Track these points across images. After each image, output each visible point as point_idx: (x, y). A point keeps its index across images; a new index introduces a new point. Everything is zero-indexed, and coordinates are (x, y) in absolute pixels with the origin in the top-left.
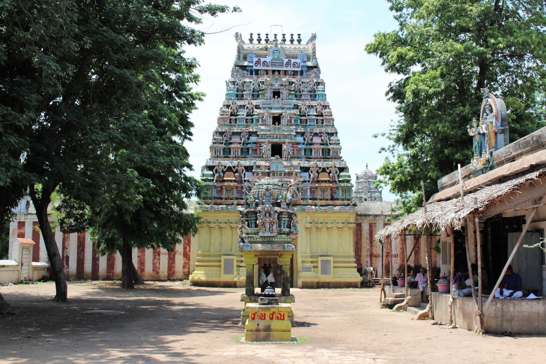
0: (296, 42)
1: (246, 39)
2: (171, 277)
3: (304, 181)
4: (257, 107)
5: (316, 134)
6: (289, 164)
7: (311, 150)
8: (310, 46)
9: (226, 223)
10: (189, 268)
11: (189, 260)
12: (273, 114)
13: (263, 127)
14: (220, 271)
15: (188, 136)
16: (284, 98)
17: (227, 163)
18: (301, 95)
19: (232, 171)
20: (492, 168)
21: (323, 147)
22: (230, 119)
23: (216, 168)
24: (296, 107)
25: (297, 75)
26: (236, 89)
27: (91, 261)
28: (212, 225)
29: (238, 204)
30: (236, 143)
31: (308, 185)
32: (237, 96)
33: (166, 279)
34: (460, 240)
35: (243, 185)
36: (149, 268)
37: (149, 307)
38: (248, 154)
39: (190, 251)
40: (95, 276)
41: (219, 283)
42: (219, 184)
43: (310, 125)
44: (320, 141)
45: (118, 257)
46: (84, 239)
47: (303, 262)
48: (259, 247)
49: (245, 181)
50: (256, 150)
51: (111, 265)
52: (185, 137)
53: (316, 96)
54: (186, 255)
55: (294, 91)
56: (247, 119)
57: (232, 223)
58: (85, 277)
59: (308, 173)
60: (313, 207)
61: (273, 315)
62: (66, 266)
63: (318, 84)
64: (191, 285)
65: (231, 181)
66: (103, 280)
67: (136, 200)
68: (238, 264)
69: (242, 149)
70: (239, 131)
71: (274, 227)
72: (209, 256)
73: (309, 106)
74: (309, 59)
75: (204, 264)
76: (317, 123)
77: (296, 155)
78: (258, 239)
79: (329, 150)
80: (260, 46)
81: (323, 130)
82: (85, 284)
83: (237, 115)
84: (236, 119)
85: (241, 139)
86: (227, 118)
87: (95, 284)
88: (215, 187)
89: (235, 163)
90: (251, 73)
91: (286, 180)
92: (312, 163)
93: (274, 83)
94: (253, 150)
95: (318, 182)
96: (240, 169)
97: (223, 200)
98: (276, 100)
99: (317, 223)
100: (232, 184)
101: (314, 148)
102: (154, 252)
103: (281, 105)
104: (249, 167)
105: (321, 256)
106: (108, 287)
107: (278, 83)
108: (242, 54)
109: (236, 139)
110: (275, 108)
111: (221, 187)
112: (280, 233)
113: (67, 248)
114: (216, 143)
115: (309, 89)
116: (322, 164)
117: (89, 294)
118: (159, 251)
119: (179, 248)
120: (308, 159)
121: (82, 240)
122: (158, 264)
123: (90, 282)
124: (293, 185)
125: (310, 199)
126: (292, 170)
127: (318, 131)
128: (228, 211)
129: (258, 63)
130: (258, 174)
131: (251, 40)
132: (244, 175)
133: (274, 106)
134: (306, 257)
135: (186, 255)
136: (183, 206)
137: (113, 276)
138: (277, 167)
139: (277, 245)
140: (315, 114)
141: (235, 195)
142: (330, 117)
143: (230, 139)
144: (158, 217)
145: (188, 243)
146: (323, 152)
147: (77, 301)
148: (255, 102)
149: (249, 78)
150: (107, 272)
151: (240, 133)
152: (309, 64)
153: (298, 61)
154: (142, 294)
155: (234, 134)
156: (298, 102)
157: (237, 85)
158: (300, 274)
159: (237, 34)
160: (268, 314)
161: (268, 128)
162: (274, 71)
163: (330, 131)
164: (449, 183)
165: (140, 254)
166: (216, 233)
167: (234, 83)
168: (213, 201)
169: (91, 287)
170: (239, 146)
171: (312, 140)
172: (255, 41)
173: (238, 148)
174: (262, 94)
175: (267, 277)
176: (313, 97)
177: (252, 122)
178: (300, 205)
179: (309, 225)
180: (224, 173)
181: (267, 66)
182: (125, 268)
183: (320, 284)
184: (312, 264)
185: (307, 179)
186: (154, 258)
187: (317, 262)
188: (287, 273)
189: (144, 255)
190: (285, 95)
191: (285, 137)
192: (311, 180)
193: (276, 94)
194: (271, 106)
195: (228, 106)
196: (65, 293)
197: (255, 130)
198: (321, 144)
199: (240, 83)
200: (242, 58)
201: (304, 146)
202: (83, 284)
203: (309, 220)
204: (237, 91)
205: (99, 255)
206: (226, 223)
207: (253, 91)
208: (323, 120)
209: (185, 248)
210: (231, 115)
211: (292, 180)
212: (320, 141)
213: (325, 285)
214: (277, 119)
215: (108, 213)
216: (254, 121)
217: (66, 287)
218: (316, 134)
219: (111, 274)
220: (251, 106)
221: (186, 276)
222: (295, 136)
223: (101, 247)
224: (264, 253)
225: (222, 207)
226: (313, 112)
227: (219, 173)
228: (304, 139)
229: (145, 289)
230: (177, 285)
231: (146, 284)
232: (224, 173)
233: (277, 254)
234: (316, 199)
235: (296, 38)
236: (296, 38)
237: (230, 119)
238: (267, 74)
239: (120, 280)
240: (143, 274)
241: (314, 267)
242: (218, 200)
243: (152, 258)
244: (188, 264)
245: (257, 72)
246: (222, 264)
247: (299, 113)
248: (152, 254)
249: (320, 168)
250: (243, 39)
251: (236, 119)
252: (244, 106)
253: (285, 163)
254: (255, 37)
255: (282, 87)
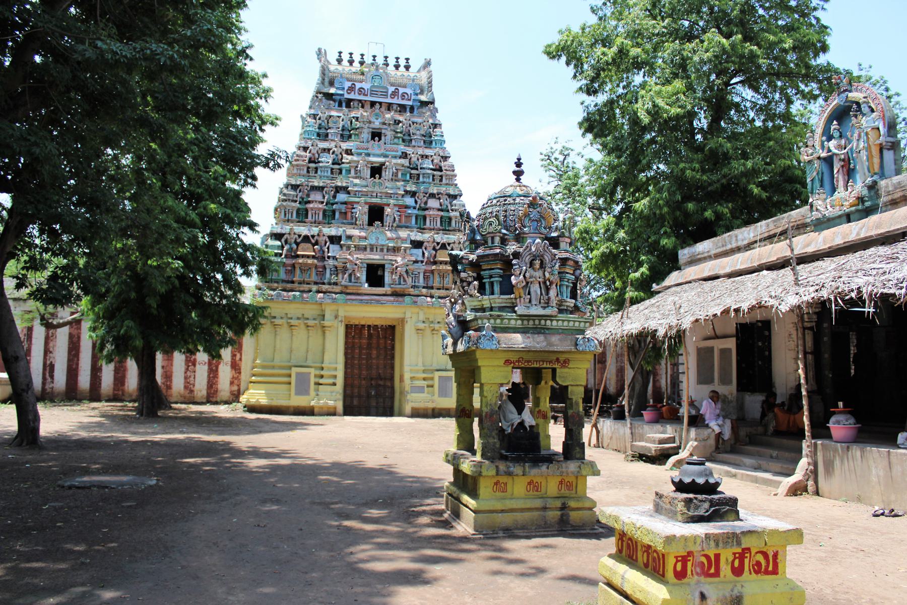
0: (402, 69)
1: (332, 58)
2: (211, 398)
3: (416, 262)
4: (349, 152)
5: (432, 196)
6: (394, 236)
7: (425, 218)
8: (424, 75)
9: (298, 318)
10: (239, 386)
11: (240, 373)
12: (372, 163)
13: (357, 181)
14: (290, 390)
15: (249, 181)
16: (388, 141)
17: (303, 230)
18: (411, 140)
19: (310, 242)
20: (868, 212)
21: (442, 213)
22: (308, 168)
23: (285, 237)
24: (405, 155)
25: (405, 111)
26: (317, 126)
27: (89, 372)
28: (277, 321)
29: (318, 292)
30: (317, 201)
31: (422, 267)
32: (318, 135)
33: (204, 401)
34: (760, 344)
35: (326, 263)
36: (178, 384)
37: (199, 460)
38: (334, 218)
39: (241, 359)
40: (94, 395)
41: (288, 408)
42: (289, 261)
43: (424, 182)
44: (438, 206)
45: (132, 366)
46: (79, 338)
47: (412, 378)
48: (518, 340)
49: (329, 257)
50: (346, 213)
51: (120, 377)
52: (246, 184)
53: (431, 142)
54: (235, 366)
55: (401, 133)
56: (332, 169)
57: (308, 319)
58: (78, 397)
59: (420, 250)
60: (429, 299)
61: (741, 557)
62: (49, 380)
63: (436, 126)
64: (245, 411)
65: (308, 257)
66: (108, 401)
67: (172, 268)
68: (317, 380)
69: (325, 211)
70: (321, 185)
71: (553, 293)
72: (273, 367)
73: (422, 156)
74: (422, 93)
75: (265, 378)
76: (433, 180)
77: (403, 223)
78: (513, 322)
79: (450, 219)
80: (354, 69)
81: (443, 189)
82: (79, 408)
83: (319, 162)
84: (316, 168)
85: (324, 197)
86: (303, 166)
87: (94, 409)
88: (284, 265)
89: (315, 230)
90: (340, 105)
91: (390, 258)
92: (425, 237)
93: (373, 119)
94: (341, 213)
95: (435, 263)
96: (322, 239)
97: (296, 285)
98: (376, 143)
99: (432, 322)
100: (310, 261)
101: (430, 216)
102: (186, 360)
103: (383, 151)
104: (336, 237)
105: (438, 370)
106: (115, 412)
107: (380, 120)
108: (328, 78)
109: (316, 196)
110: (375, 155)
111: (293, 266)
112: (561, 311)
113: (51, 352)
114: (286, 200)
115: (423, 132)
116: (441, 238)
117: (83, 427)
118: (195, 360)
119: (226, 353)
120: (422, 230)
121: (75, 339)
122: (192, 379)
123: (87, 405)
124: (401, 266)
125: (424, 287)
126: (399, 244)
127: (435, 192)
128: (303, 301)
129: (351, 89)
130: (349, 248)
131: (340, 61)
132: (328, 248)
133: (373, 152)
134: (417, 371)
135: (235, 366)
136: (238, 289)
137: (123, 395)
138: (377, 239)
139: (558, 337)
140: (431, 167)
141: (314, 278)
142: (452, 173)
143: (308, 196)
144: (200, 304)
145: (238, 347)
146: (441, 222)
147: (61, 443)
148: (345, 146)
149: (338, 111)
150: (114, 389)
151: (323, 188)
152: (423, 98)
153: (409, 91)
154: (173, 427)
155: (314, 188)
156: (407, 148)
157: (320, 119)
158: (409, 397)
159: (320, 50)
160: (727, 555)
161: (364, 183)
162: (373, 104)
163: (452, 193)
164: (713, 252)
165: (165, 363)
166: (284, 333)
167: (314, 116)
168: (281, 286)
169: (88, 413)
170: (321, 206)
171: (426, 203)
172: (345, 63)
173: (319, 209)
174: (355, 135)
175: (520, 413)
176: (429, 143)
177: (341, 173)
178: (409, 295)
179: (421, 326)
180: (297, 244)
181: (364, 95)
182: (144, 383)
183: (436, 411)
184: (426, 383)
185: (420, 258)
186: (187, 369)
187: (432, 379)
188: (577, 404)
189: (172, 365)
190: (389, 137)
191: (389, 196)
192: (425, 260)
193: (376, 135)
194: (369, 151)
195: (305, 149)
196: (36, 430)
197: (344, 185)
198: (439, 210)
199: (324, 116)
200: (327, 83)
201: (416, 212)
202: (74, 408)
203: (422, 317)
204: (319, 128)
205: (103, 363)
206: (298, 318)
207: (343, 130)
208: (441, 176)
209: (234, 356)
210: (310, 161)
211: (399, 259)
212: (438, 206)
213: (444, 412)
214: (376, 171)
215: (120, 294)
216: (344, 172)
217: (37, 418)
218: (432, 196)
219: (120, 393)
220: (340, 150)
221: (235, 397)
222: (403, 196)
223: (106, 350)
224: (526, 357)
225: (294, 295)
226: (428, 164)
227: (290, 244)
228: (416, 202)
229: (176, 418)
230: (222, 411)
231: (175, 409)
232: (297, 244)
233: (558, 359)
234: (432, 288)
235: (402, 63)
236: (402, 63)
237: (308, 168)
238: (363, 107)
239: (134, 401)
240: (169, 393)
241: (428, 386)
242: (288, 284)
243: (183, 370)
244: (238, 379)
245: (349, 103)
246: (293, 380)
247: (408, 164)
248: (183, 364)
249: (438, 243)
250: (328, 58)
251: (316, 168)
252: (329, 150)
253: (389, 234)
254: (345, 57)
255: (385, 127)
